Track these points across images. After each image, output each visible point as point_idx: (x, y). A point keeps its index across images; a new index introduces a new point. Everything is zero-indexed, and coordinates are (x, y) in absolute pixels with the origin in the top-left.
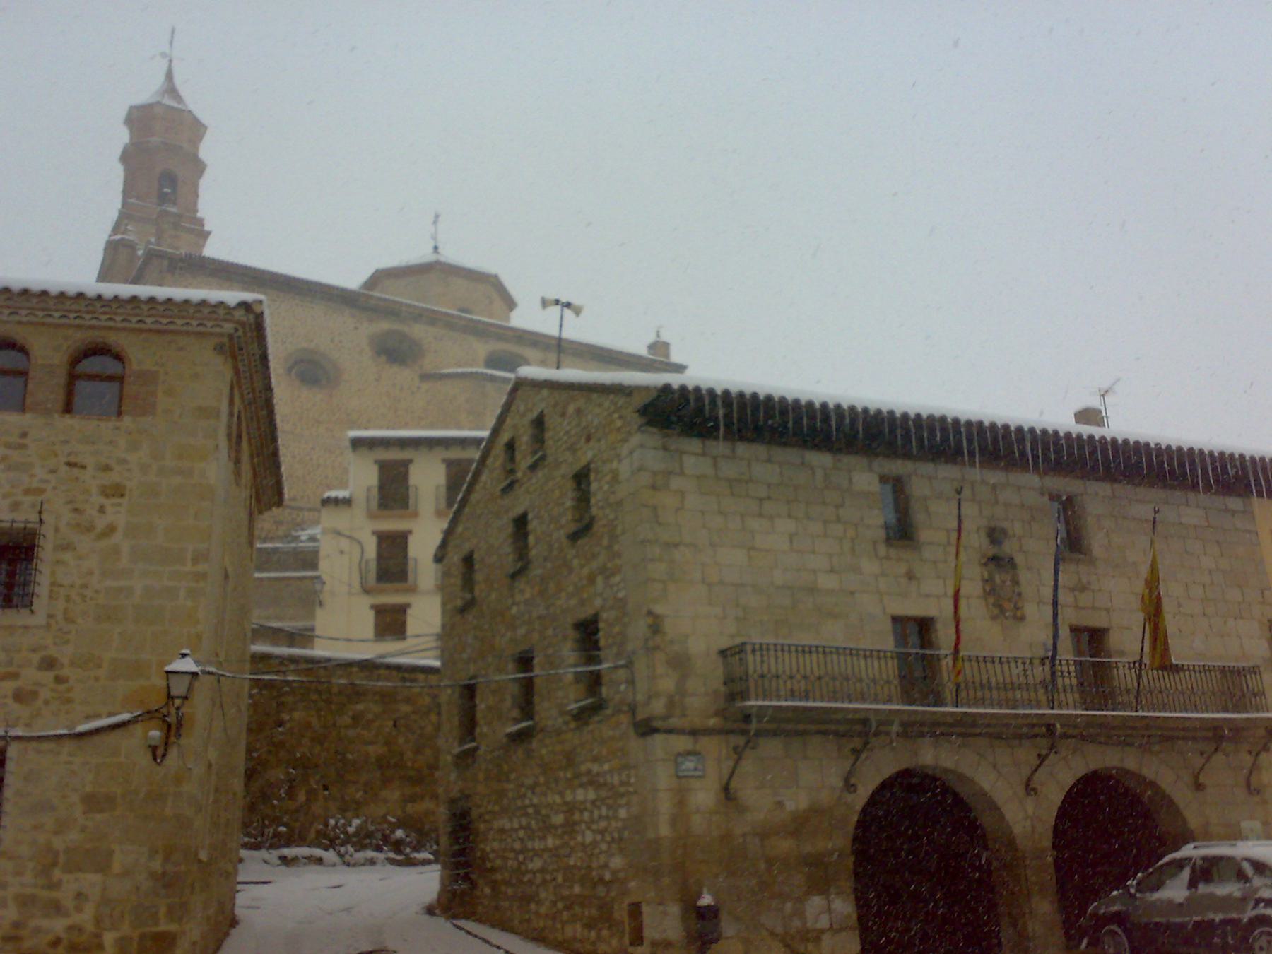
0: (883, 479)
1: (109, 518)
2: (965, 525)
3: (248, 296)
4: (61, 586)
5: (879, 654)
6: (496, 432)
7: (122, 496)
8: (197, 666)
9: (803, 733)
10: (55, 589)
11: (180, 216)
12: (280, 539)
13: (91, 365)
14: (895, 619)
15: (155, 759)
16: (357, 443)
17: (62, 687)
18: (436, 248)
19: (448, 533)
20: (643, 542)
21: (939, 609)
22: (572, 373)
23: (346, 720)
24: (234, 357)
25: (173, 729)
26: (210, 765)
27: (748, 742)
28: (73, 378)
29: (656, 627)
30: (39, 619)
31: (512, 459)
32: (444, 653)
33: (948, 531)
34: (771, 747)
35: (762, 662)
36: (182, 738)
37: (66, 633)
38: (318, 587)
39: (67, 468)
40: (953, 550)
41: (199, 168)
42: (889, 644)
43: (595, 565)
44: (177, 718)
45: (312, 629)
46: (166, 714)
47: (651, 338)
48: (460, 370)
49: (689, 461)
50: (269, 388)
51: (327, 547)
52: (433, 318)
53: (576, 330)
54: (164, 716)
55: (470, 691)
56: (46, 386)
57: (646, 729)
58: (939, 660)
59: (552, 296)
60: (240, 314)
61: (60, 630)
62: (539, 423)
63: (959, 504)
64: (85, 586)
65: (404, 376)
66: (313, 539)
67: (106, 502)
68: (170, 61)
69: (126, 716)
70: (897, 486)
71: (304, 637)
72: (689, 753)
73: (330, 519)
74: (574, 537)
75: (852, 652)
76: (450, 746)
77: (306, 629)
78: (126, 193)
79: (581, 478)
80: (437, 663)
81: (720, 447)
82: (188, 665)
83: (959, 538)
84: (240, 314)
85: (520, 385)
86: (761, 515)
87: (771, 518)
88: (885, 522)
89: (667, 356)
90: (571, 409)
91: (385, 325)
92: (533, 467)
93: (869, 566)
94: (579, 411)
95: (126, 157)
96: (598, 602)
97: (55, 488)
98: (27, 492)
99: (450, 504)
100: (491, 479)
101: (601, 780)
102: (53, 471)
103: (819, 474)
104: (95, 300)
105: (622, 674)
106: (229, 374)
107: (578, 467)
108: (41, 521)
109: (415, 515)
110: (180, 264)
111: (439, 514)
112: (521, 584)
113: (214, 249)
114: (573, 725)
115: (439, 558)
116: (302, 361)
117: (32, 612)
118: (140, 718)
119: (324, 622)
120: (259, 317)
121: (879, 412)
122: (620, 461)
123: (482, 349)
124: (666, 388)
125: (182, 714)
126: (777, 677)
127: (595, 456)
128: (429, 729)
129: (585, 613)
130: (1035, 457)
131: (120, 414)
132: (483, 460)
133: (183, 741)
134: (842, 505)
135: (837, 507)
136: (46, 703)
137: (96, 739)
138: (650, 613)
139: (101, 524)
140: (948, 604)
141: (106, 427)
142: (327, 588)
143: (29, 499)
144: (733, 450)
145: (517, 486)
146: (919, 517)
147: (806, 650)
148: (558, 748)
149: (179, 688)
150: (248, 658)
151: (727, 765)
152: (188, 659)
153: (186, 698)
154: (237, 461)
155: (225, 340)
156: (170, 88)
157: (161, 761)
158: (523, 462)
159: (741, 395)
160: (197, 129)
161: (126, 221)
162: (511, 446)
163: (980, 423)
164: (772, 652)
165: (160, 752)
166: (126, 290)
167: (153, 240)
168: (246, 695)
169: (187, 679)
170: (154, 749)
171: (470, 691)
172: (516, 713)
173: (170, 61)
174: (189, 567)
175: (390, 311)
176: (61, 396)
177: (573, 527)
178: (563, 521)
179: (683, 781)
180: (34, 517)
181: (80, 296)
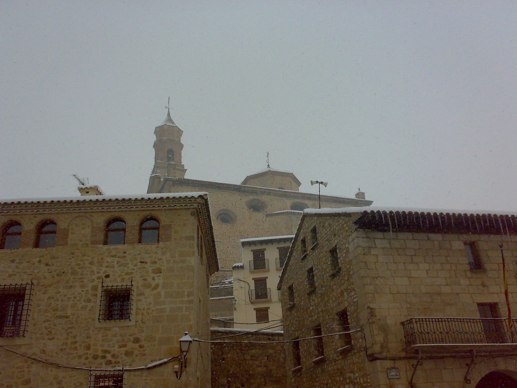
0: (465, 244)
1: (156, 281)
2: (506, 261)
3: (202, 193)
4: (140, 309)
5: (474, 321)
6: (297, 235)
7: (161, 272)
8: (191, 338)
9: (443, 357)
10: (138, 311)
11: (175, 165)
12: (218, 284)
13: (147, 224)
14: (479, 304)
15: (177, 377)
16: (244, 244)
17: (142, 349)
18: (268, 166)
19: (282, 278)
20: (362, 277)
21: (499, 299)
22: (326, 210)
23: (248, 357)
24: (198, 216)
25: (184, 365)
26: (198, 378)
27: (418, 362)
28: (141, 230)
29: (372, 312)
30: (133, 323)
31: (304, 246)
32: (285, 327)
33: (498, 264)
34: (428, 365)
35: (421, 327)
36: (187, 368)
37: (142, 328)
38: (234, 302)
39: (141, 264)
40: (502, 271)
41: (181, 146)
42: (477, 316)
43: (343, 287)
44: (185, 360)
45: (233, 320)
46: (180, 358)
47: (357, 191)
48: (281, 212)
49: (378, 242)
50: (211, 228)
51: (236, 285)
52: (269, 193)
53: (325, 192)
54: (180, 359)
55: (296, 344)
56: (132, 233)
57: (373, 358)
58: (502, 322)
59: (314, 180)
60: (199, 200)
61: (140, 327)
62: (314, 230)
63: (502, 251)
64: (149, 309)
65: (259, 216)
66: (230, 283)
67: (155, 275)
68: (169, 109)
69: (166, 360)
70: (472, 245)
71: (229, 323)
72: (393, 368)
73: (236, 274)
74: (333, 276)
75: (461, 321)
76: (290, 367)
77: (230, 320)
78: (156, 159)
79: (333, 252)
80: (282, 332)
81: (391, 234)
82: (188, 338)
83: (504, 266)
84: (199, 200)
85: (305, 216)
86: (412, 262)
87: (417, 263)
88: (469, 262)
89: (364, 198)
90: (327, 224)
91: (251, 197)
92: (313, 249)
93: (464, 282)
94: (330, 225)
95: (155, 146)
96: (346, 304)
97: (136, 272)
98: (127, 274)
99: (281, 266)
100: (297, 255)
101: (355, 381)
102: (136, 265)
103: (436, 243)
104: (148, 200)
105: (359, 334)
106: (197, 223)
107: (331, 248)
108: (132, 285)
109: (268, 271)
110: (176, 182)
111: (277, 270)
112: (313, 297)
113: (188, 176)
114: (341, 357)
115: (279, 289)
116: (221, 214)
117: (130, 320)
118: (171, 360)
119: (237, 316)
120: (206, 201)
121: (460, 215)
122: (349, 244)
123: (289, 202)
124: (365, 212)
125: (187, 358)
126: (428, 333)
127: (337, 243)
128: (281, 360)
129: (341, 308)
130: (504, 227)
131: (158, 241)
132: (293, 247)
133: (187, 369)
134: (449, 256)
135: (447, 257)
136: (136, 356)
137: (156, 369)
138: (369, 307)
139: (153, 284)
140: (503, 296)
141: (153, 247)
142: (237, 302)
143: (127, 277)
144: (397, 236)
145: (308, 257)
146: (484, 259)
147: (439, 320)
148: (335, 367)
149: (185, 347)
150: (210, 333)
151: (410, 374)
152: (188, 335)
153: (187, 352)
154: (201, 256)
155: (195, 210)
156: (170, 119)
157: (180, 378)
158: (309, 248)
159: (398, 212)
160: (180, 132)
161: (157, 169)
162: (304, 241)
163: (507, 216)
164: (424, 322)
165: (179, 374)
166: (158, 195)
167: (166, 174)
168: (210, 348)
169: (188, 343)
170: (176, 372)
171: (296, 344)
172: (316, 353)
173: (169, 109)
174: (186, 299)
175: (254, 191)
176: (137, 236)
177: (332, 272)
178: (328, 270)
179: (391, 380)
180: (129, 284)
181: (143, 199)
